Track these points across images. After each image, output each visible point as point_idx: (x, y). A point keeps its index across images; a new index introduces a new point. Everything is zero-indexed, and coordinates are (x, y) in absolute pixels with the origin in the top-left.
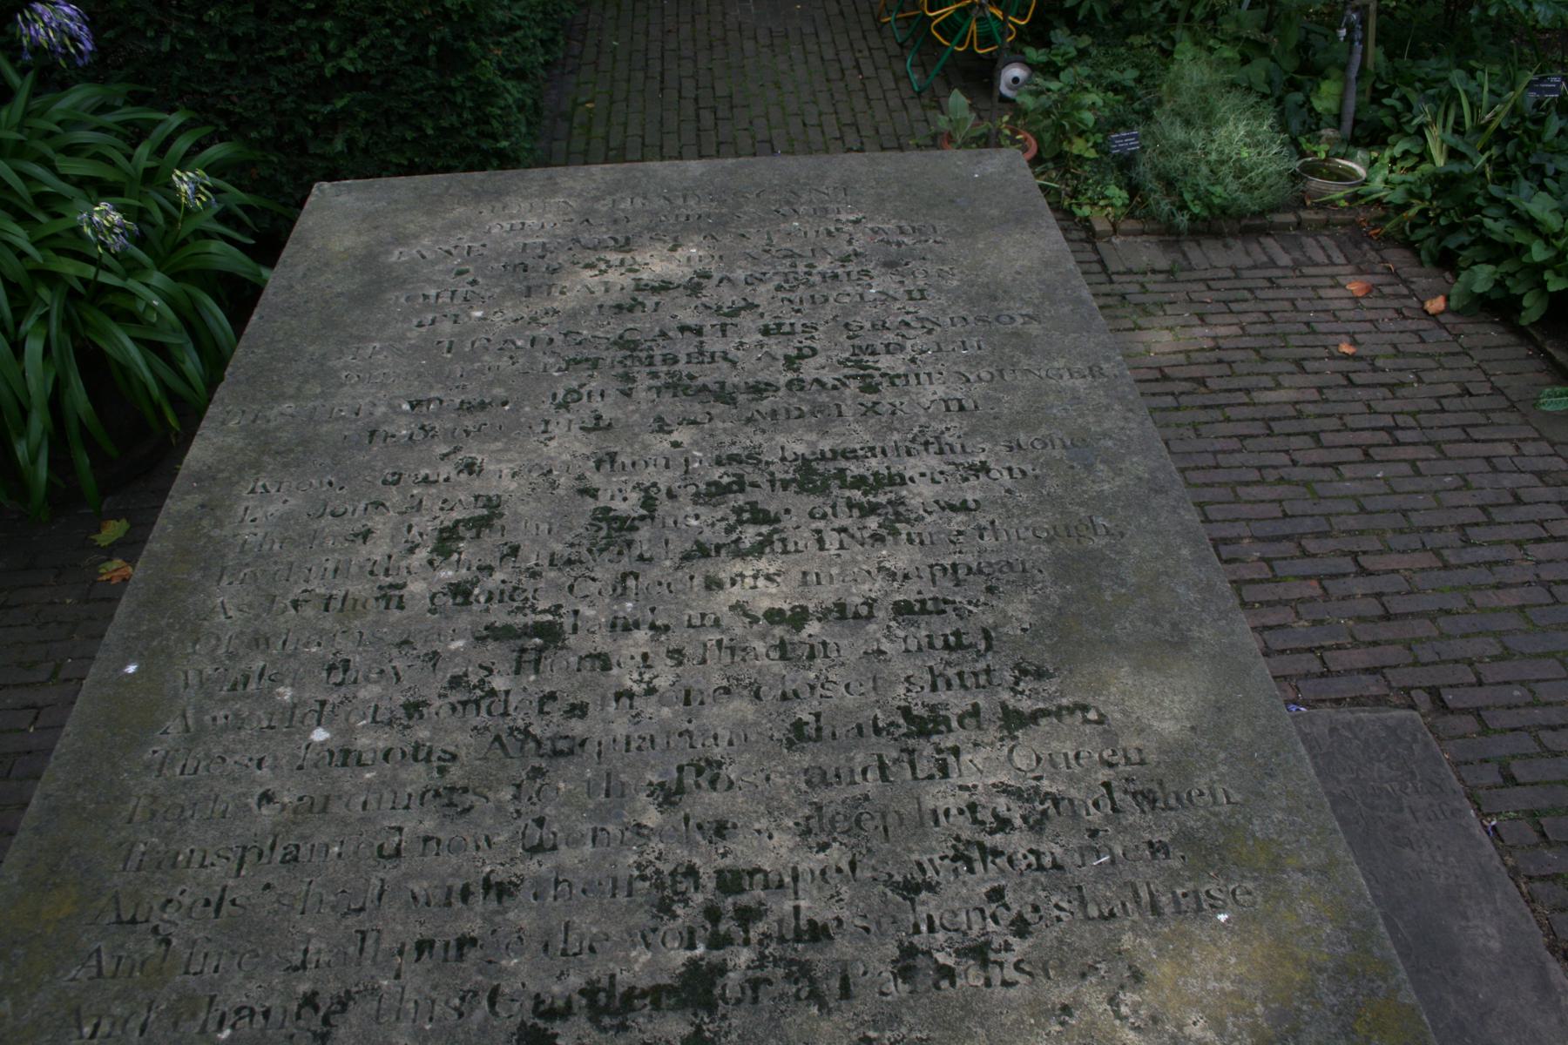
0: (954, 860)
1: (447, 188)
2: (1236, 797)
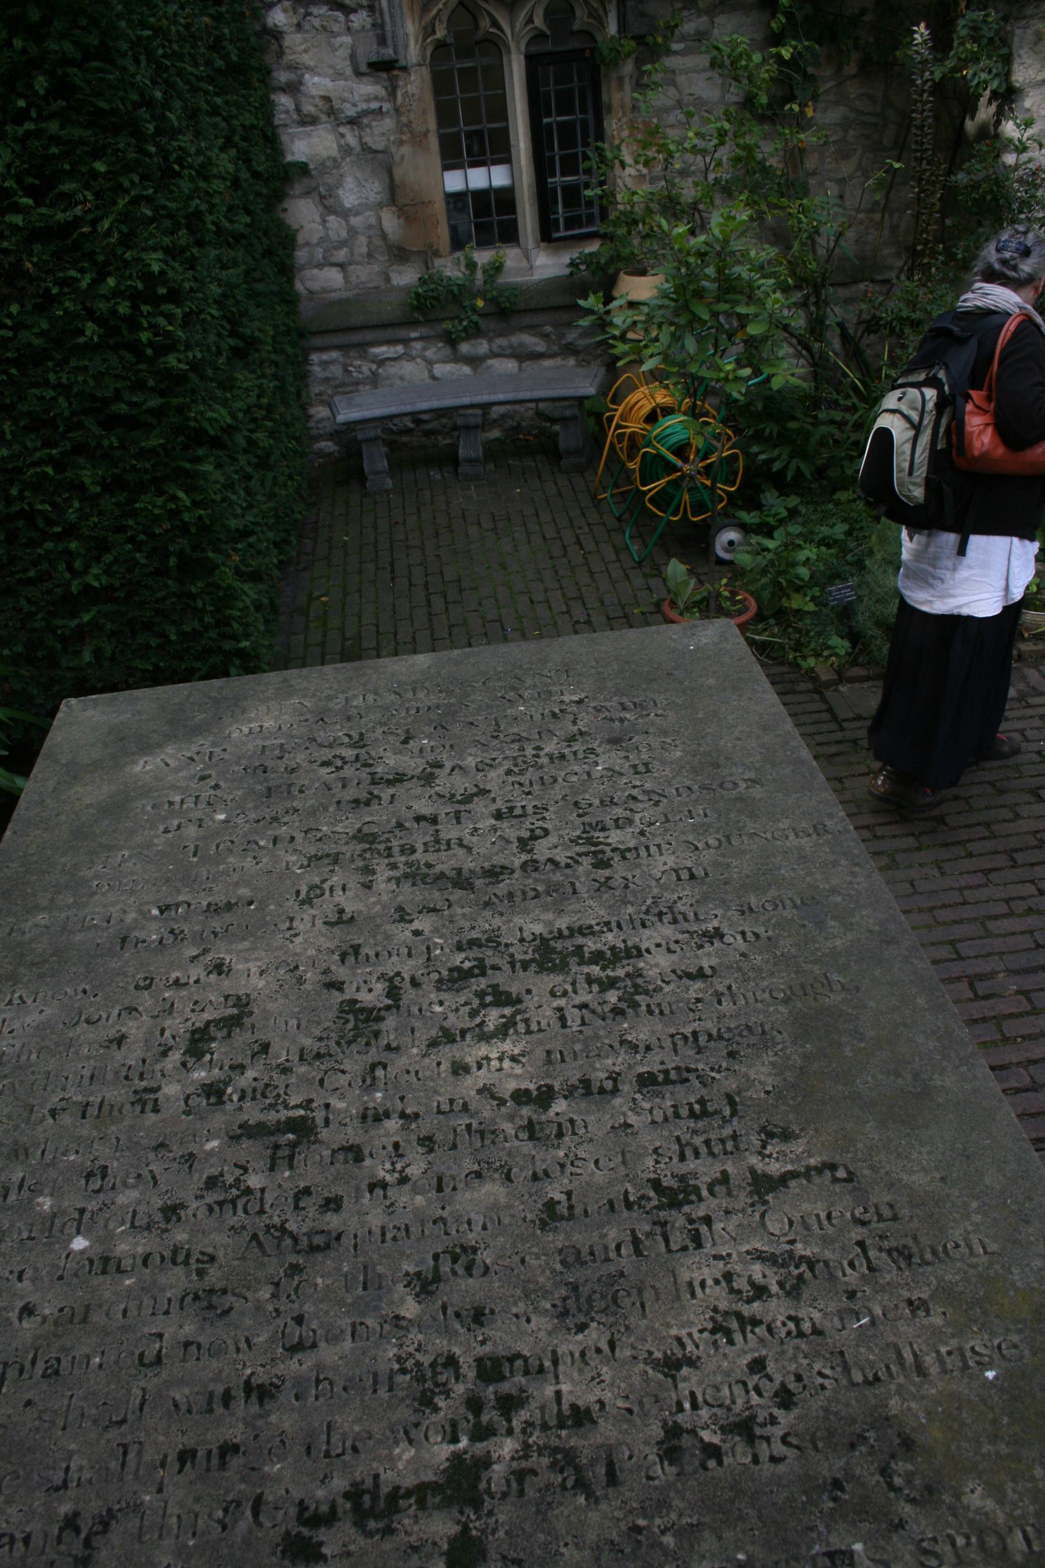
0: (713, 1332)
1: (188, 697)
2: (993, 1247)
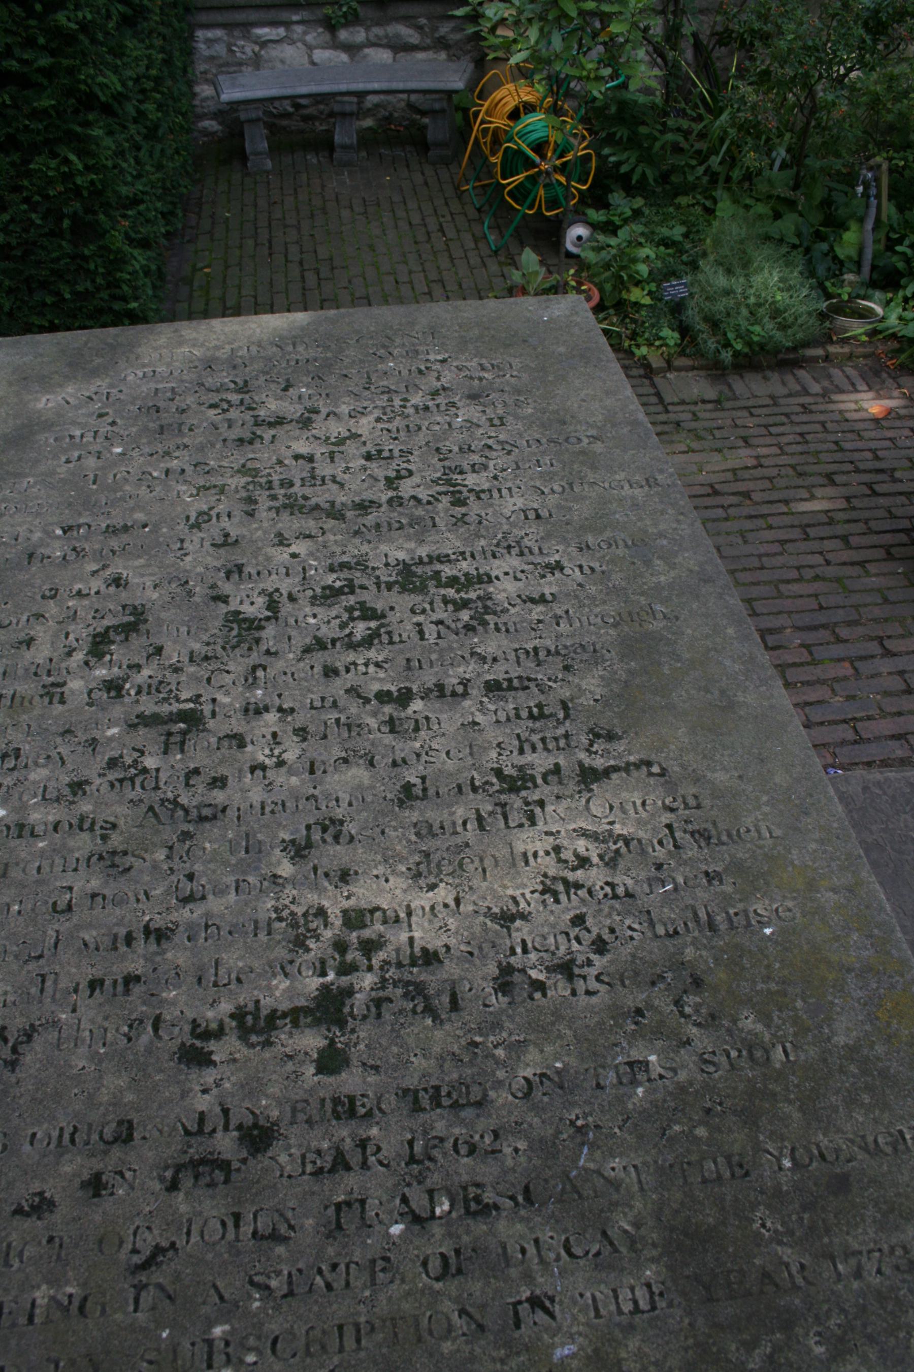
0: (543, 893)
1: (86, 343)
2: (778, 832)
